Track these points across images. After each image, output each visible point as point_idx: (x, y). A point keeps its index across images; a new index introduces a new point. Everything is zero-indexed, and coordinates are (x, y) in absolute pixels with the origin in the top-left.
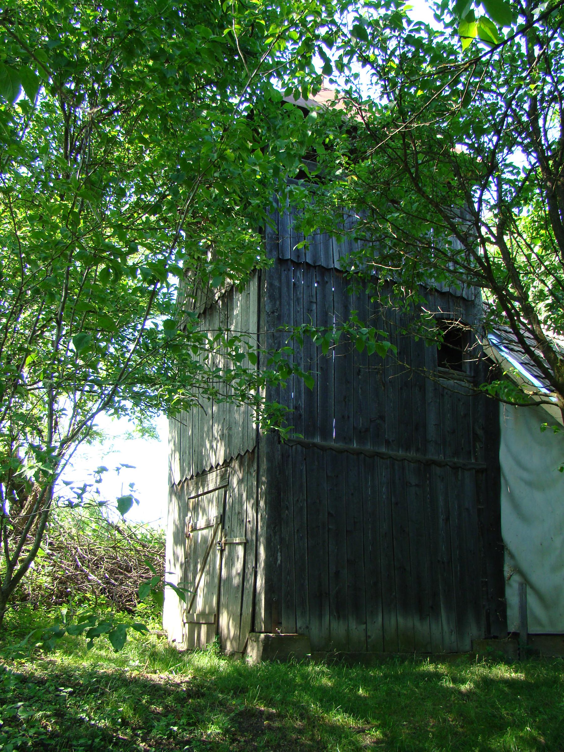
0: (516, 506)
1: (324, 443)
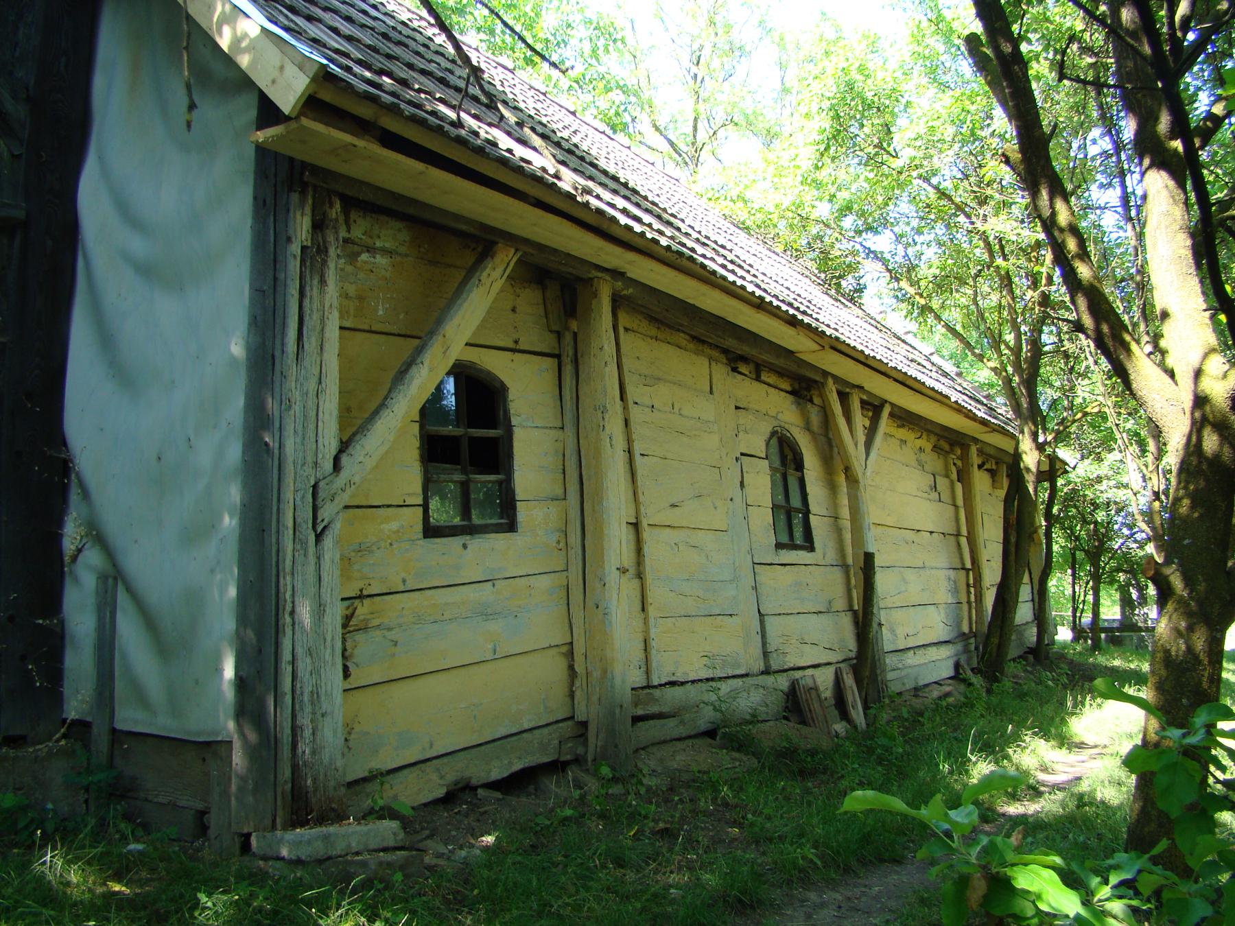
0: (106, 340)
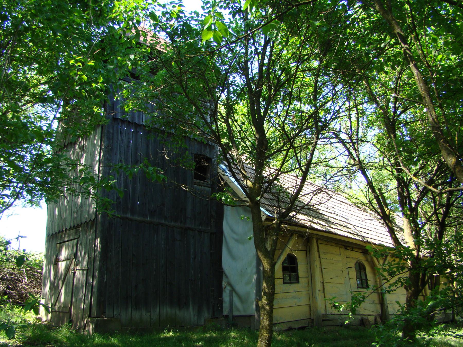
1: (132, 217)
